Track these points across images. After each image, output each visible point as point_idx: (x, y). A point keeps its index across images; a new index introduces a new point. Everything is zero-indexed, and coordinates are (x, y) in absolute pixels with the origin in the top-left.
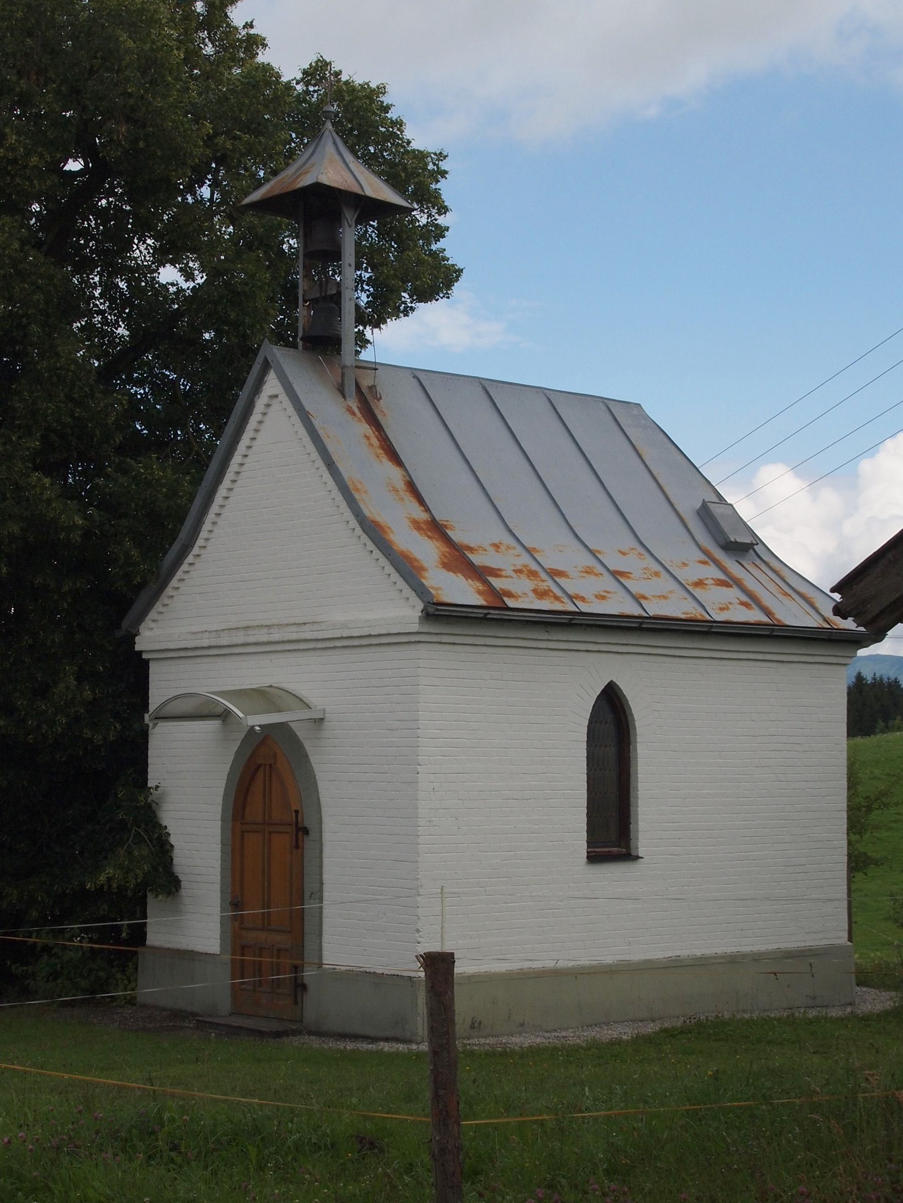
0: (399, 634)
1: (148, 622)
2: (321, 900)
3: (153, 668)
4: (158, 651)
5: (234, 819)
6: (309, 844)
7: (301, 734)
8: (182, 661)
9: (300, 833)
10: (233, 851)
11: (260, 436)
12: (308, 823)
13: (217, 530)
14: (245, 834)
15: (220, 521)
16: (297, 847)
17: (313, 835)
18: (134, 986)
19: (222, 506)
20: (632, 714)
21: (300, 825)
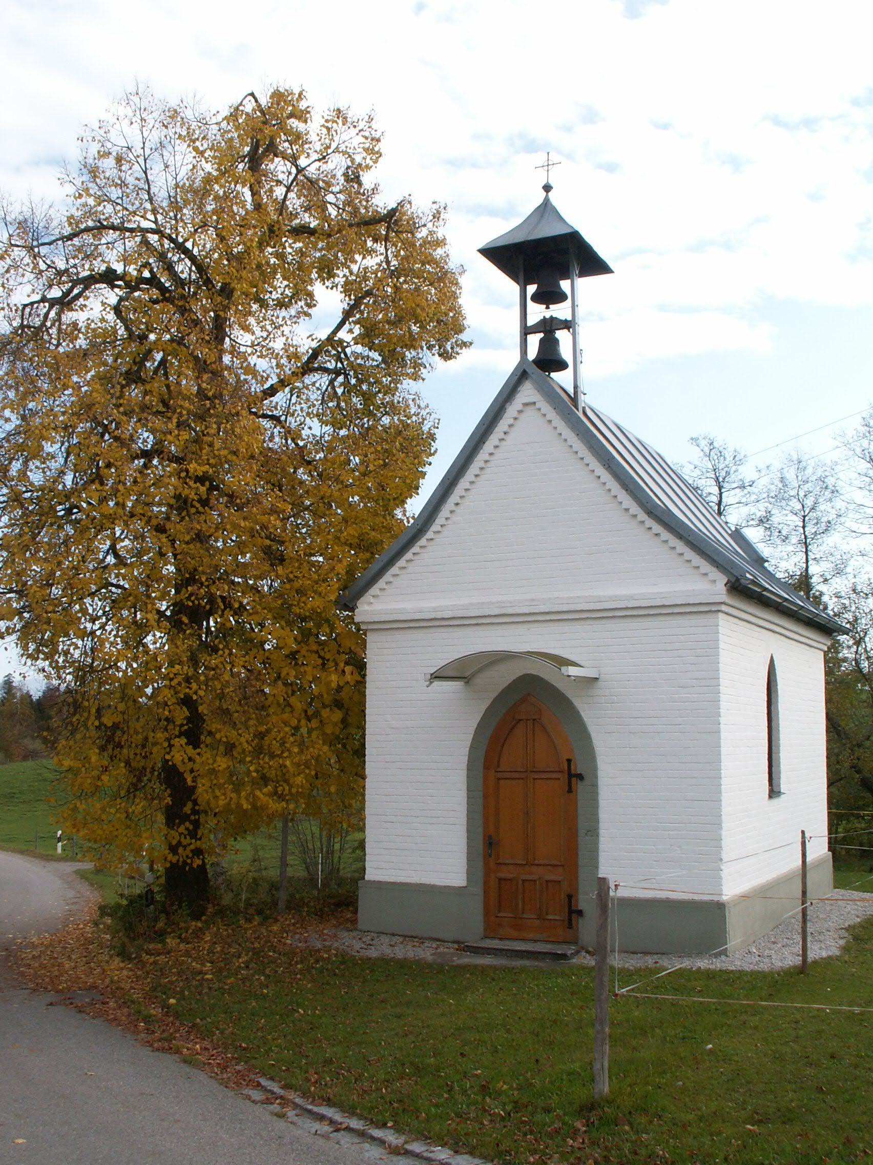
0: (700, 604)
1: (368, 597)
2: (830, 839)
3: (371, 638)
4: (374, 622)
5: (486, 767)
6: (581, 788)
7: (569, 694)
8: (410, 631)
9: (574, 779)
10: (485, 796)
11: (509, 438)
12: (579, 768)
13: (454, 518)
14: (501, 782)
15: (459, 510)
16: (570, 791)
17: (587, 781)
18: (569, 952)
19: (462, 497)
20: (777, 691)
21: (573, 772)
